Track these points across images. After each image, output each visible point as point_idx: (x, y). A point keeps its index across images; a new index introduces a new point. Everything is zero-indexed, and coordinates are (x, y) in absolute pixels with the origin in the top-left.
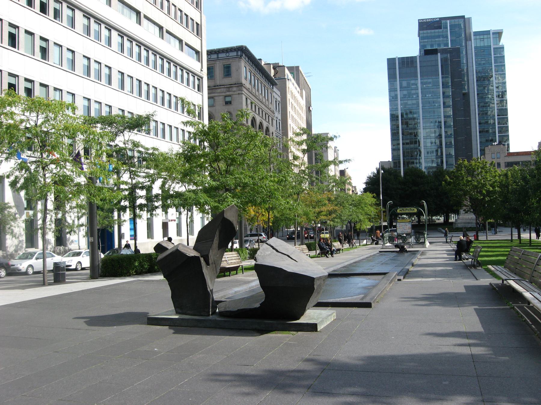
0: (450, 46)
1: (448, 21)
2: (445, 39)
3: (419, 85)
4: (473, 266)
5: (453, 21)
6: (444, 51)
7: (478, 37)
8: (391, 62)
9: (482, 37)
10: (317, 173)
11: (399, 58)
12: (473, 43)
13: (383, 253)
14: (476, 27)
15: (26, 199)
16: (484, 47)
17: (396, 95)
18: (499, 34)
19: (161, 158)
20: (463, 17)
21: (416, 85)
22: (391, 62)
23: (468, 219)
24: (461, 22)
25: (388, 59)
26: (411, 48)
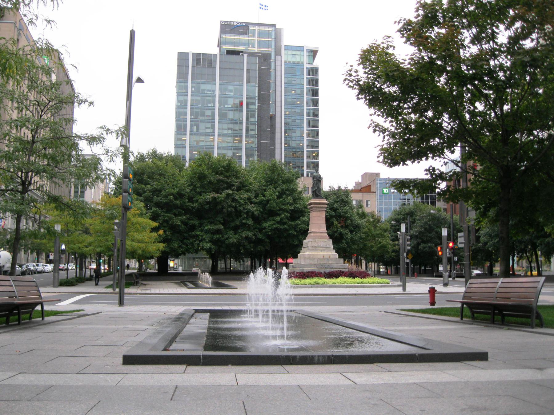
2: (237, 127)
3: (217, 93)
5: (262, 28)
6: (252, 54)
7: (290, 52)
8: (182, 57)
9: (294, 53)
11: (193, 53)
12: (286, 57)
13: (176, 297)
14: (286, 41)
16: (298, 63)
17: (186, 101)
18: (314, 53)
19: (305, 218)
20: (274, 26)
21: (214, 91)
22: (182, 57)
23: (323, 259)
25: (179, 53)
26: (209, 44)
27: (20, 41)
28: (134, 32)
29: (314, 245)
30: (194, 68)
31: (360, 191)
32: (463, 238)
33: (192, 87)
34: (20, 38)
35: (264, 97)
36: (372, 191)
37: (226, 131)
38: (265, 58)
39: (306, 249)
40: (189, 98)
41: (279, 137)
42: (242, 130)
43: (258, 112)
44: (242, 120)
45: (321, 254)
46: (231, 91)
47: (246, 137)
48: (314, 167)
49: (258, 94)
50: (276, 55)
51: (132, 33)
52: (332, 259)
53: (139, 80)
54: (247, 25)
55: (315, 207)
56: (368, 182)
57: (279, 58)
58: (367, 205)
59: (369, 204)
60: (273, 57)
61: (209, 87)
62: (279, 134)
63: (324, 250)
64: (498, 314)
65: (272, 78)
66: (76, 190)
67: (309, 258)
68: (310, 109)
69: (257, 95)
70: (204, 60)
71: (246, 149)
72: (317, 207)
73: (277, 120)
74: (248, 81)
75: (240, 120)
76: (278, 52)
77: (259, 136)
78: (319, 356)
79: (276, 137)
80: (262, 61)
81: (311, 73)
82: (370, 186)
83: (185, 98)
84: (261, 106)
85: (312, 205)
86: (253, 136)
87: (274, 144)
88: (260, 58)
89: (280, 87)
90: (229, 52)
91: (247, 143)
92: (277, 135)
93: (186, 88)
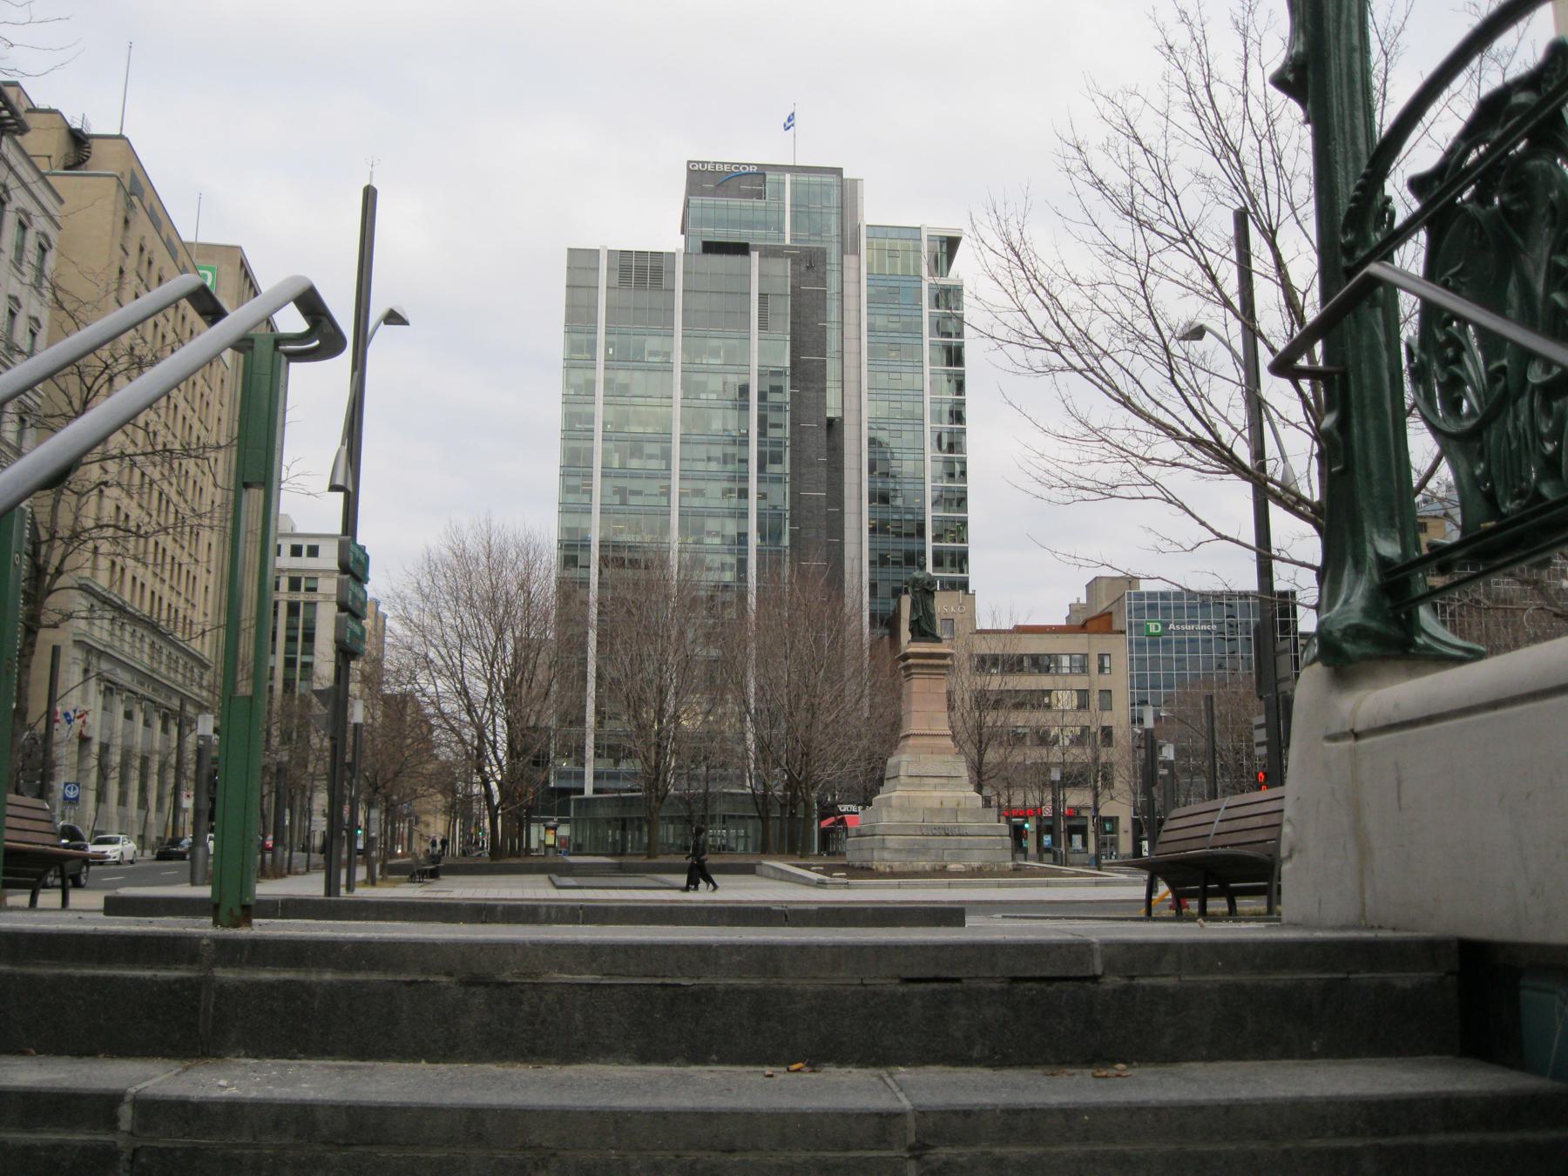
0: (788, 242)
1: (788, 177)
3: (678, 358)
4: (101, 654)
5: (803, 178)
6: (770, 253)
8: (581, 262)
10: (290, 738)
14: (874, 211)
15: (386, 972)
17: (591, 384)
20: (838, 172)
21: (668, 354)
22: (581, 262)
23: (940, 810)
24: (831, 179)
25: (570, 250)
26: (660, 228)
27: (131, 224)
28: (375, 191)
29: (914, 771)
30: (619, 294)
31: (1084, 628)
32: (1263, 731)
33: (608, 345)
34: (131, 216)
35: (807, 369)
36: (1116, 626)
37: (700, 466)
38: (810, 263)
39: (892, 782)
40: (600, 374)
41: (855, 480)
42: (746, 461)
43: (792, 412)
44: (747, 435)
45: (931, 796)
46: (715, 353)
47: (760, 480)
48: (953, 564)
49: (792, 362)
50: (843, 252)
51: (370, 195)
52: (965, 811)
53: (393, 318)
54: (761, 172)
55: (917, 666)
56: (1105, 605)
57: (850, 260)
58: (1101, 669)
59: (1107, 664)
60: (833, 257)
61: (653, 343)
62: (855, 473)
63: (943, 785)
64: (1216, 894)
65: (833, 316)
66: (292, 633)
67: (902, 809)
68: (941, 402)
69: (788, 364)
70: (641, 270)
71: (759, 515)
72: (923, 666)
73: (849, 432)
74: (763, 325)
75: (742, 435)
76: (849, 244)
77: (796, 475)
78: (548, 907)
79: (846, 479)
80: (803, 268)
81: (942, 302)
82: (1110, 614)
83: (589, 373)
84: (799, 395)
85: (910, 661)
86: (778, 479)
87: (840, 502)
88: (796, 261)
89: (855, 342)
90: (710, 248)
91: (762, 496)
92: (850, 476)
93: (592, 346)
